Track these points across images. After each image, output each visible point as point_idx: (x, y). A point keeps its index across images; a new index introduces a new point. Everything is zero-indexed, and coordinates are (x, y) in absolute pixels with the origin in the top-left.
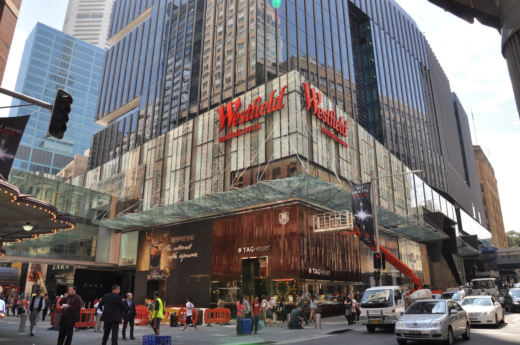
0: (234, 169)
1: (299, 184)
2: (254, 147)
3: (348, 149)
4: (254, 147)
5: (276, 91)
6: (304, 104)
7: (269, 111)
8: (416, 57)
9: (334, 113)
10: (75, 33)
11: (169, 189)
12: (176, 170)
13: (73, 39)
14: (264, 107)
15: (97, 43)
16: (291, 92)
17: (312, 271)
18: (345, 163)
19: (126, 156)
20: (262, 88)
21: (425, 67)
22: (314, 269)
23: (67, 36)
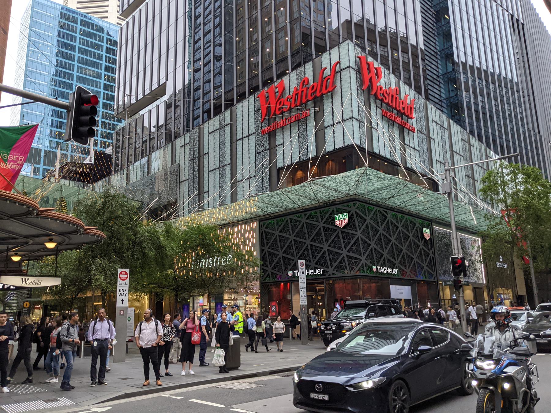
0: (280, 165)
1: (357, 179)
2: (303, 139)
3: (415, 134)
4: (303, 139)
5: (326, 68)
6: (361, 82)
7: (318, 94)
8: (505, 7)
9: (398, 91)
10: (79, 5)
11: (208, 192)
12: (214, 169)
13: (77, 14)
14: (312, 90)
15: (107, 17)
16: (344, 69)
17: (377, 269)
18: (412, 150)
19: (155, 155)
20: (309, 67)
21: (518, 20)
22: (379, 267)
23: (70, 10)
